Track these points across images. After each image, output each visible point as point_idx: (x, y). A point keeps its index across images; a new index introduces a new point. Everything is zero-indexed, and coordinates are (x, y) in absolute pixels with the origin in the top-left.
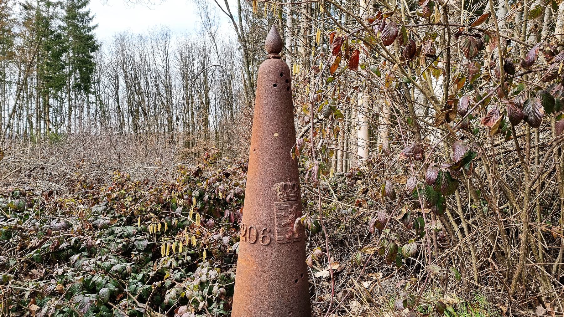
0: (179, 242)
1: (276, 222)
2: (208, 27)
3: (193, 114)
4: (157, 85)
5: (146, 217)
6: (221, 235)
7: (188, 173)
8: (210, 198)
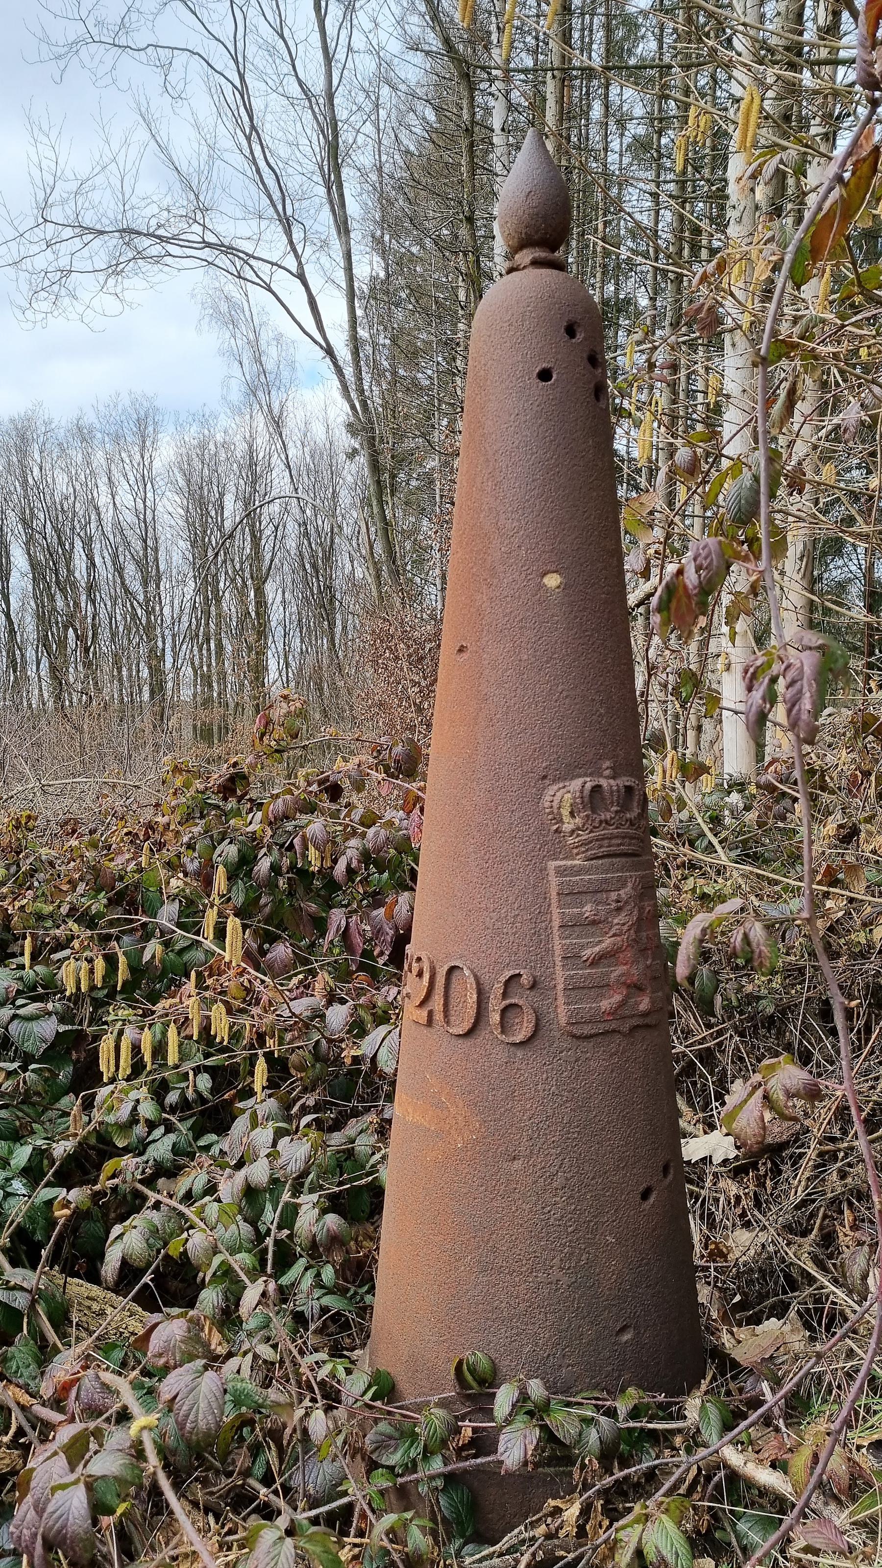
0: (166, 1025)
1: (557, 945)
2: (260, 394)
3: (220, 647)
4: (120, 570)
5: (55, 938)
6: (317, 999)
7: (199, 785)
8: (275, 868)
